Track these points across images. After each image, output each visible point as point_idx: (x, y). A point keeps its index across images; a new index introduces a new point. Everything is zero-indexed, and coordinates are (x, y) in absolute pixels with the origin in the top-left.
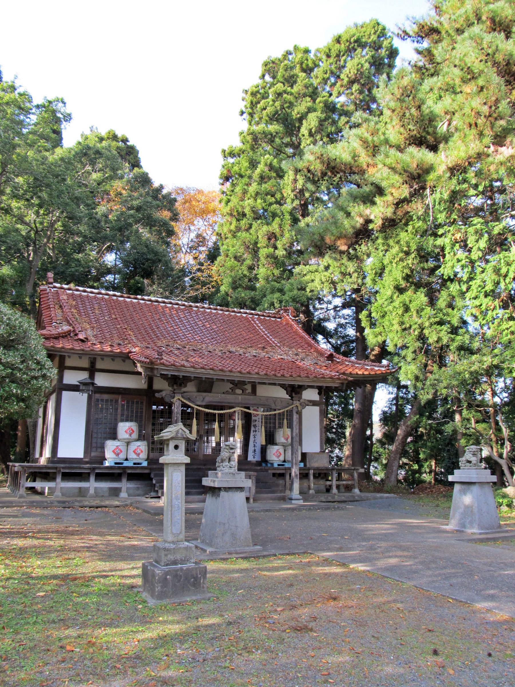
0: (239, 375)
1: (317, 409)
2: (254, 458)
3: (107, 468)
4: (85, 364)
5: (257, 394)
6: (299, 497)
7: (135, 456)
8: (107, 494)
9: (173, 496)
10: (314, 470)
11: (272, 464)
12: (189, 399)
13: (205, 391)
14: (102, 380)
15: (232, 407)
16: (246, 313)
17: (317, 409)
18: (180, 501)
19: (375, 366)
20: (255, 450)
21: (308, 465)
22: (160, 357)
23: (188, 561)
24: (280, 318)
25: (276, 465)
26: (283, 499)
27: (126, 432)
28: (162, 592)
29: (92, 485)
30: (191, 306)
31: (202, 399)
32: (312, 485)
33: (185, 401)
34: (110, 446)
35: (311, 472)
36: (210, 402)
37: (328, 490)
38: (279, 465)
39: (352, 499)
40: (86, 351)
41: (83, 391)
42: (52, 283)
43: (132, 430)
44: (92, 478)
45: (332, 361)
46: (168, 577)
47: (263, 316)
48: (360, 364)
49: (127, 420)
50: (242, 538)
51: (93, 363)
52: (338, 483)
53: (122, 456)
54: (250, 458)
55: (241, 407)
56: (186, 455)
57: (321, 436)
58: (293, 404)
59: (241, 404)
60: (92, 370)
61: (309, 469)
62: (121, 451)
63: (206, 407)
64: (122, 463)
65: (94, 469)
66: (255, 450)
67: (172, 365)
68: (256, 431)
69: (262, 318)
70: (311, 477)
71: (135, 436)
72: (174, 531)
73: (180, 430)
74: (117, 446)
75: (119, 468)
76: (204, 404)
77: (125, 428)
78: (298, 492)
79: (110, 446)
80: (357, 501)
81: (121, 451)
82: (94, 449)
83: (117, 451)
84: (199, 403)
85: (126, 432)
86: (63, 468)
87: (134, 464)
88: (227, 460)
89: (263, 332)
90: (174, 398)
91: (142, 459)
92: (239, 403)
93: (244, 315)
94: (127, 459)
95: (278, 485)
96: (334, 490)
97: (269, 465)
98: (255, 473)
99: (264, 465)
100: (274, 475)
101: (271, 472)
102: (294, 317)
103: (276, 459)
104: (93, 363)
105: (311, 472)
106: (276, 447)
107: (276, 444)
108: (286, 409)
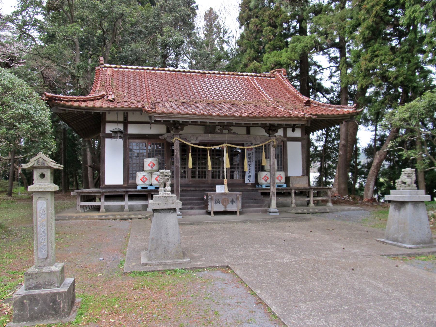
0: (218, 118)
1: (299, 144)
2: (250, 181)
3: (139, 191)
4: (121, 119)
5: (251, 133)
6: (276, 210)
7: (157, 182)
8: (141, 209)
9: (38, 223)
10: (295, 189)
11: (261, 186)
12: (185, 139)
13: (210, 133)
14: (132, 130)
15: (223, 143)
16: (247, 75)
17: (299, 144)
18: (45, 228)
19: (344, 108)
20: (250, 176)
21: (291, 186)
22: (153, 107)
23: (51, 285)
24: (274, 77)
25: (264, 187)
26: (266, 211)
27: (149, 165)
28: (19, 315)
29: (127, 203)
30: (204, 73)
31: (195, 138)
32: (294, 201)
33: (182, 141)
34: (140, 175)
35: (293, 191)
36: (203, 140)
37: (308, 203)
38: (266, 186)
39: (323, 211)
40: (112, 108)
41: (116, 138)
42: (102, 64)
43: (153, 164)
44: (126, 198)
45: (309, 106)
46: (25, 301)
47: (261, 76)
48: (332, 107)
49: (149, 157)
50: (173, 251)
51: (126, 117)
52: (315, 199)
53: (147, 182)
54: (247, 181)
55: (228, 143)
56: (55, 183)
57: (303, 164)
58: (270, 139)
59: (228, 141)
60: (126, 123)
61: (291, 189)
62: (147, 179)
63: (198, 144)
64: (147, 188)
65: (127, 192)
66: (250, 176)
67: (162, 113)
68: (250, 162)
69: (260, 78)
70: (293, 195)
71: (155, 168)
72: (40, 256)
73: (40, 159)
74: (144, 176)
75: (145, 191)
76: (197, 142)
77: (148, 162)
78: (275, 207)
79: (140, 175)
80: (327, 212)
81: (147, 179)
82: (131, 179)
83: (144, 179)
84: (194, 142)
85: (149, 165)
86: (105, 192)
87: (142, 188)
88: (163, 186)
89: (258, 88)
90: (173, 138)
91: (147, 185)
92: (225, 141)
93: (246, 77)
94: (151, 185)
95: (263, 202)
96: (312, 204)
97: (260, 186)
98: (241, 193)
99: (257, 186)
100: (262, 194)
101: (260, 191)
102: (285, 75)
103: (264, 182)
104: (126, 117)
105: (293, 191)
106: (264, 174)
107: (265, 171)
108: (265, 143)
